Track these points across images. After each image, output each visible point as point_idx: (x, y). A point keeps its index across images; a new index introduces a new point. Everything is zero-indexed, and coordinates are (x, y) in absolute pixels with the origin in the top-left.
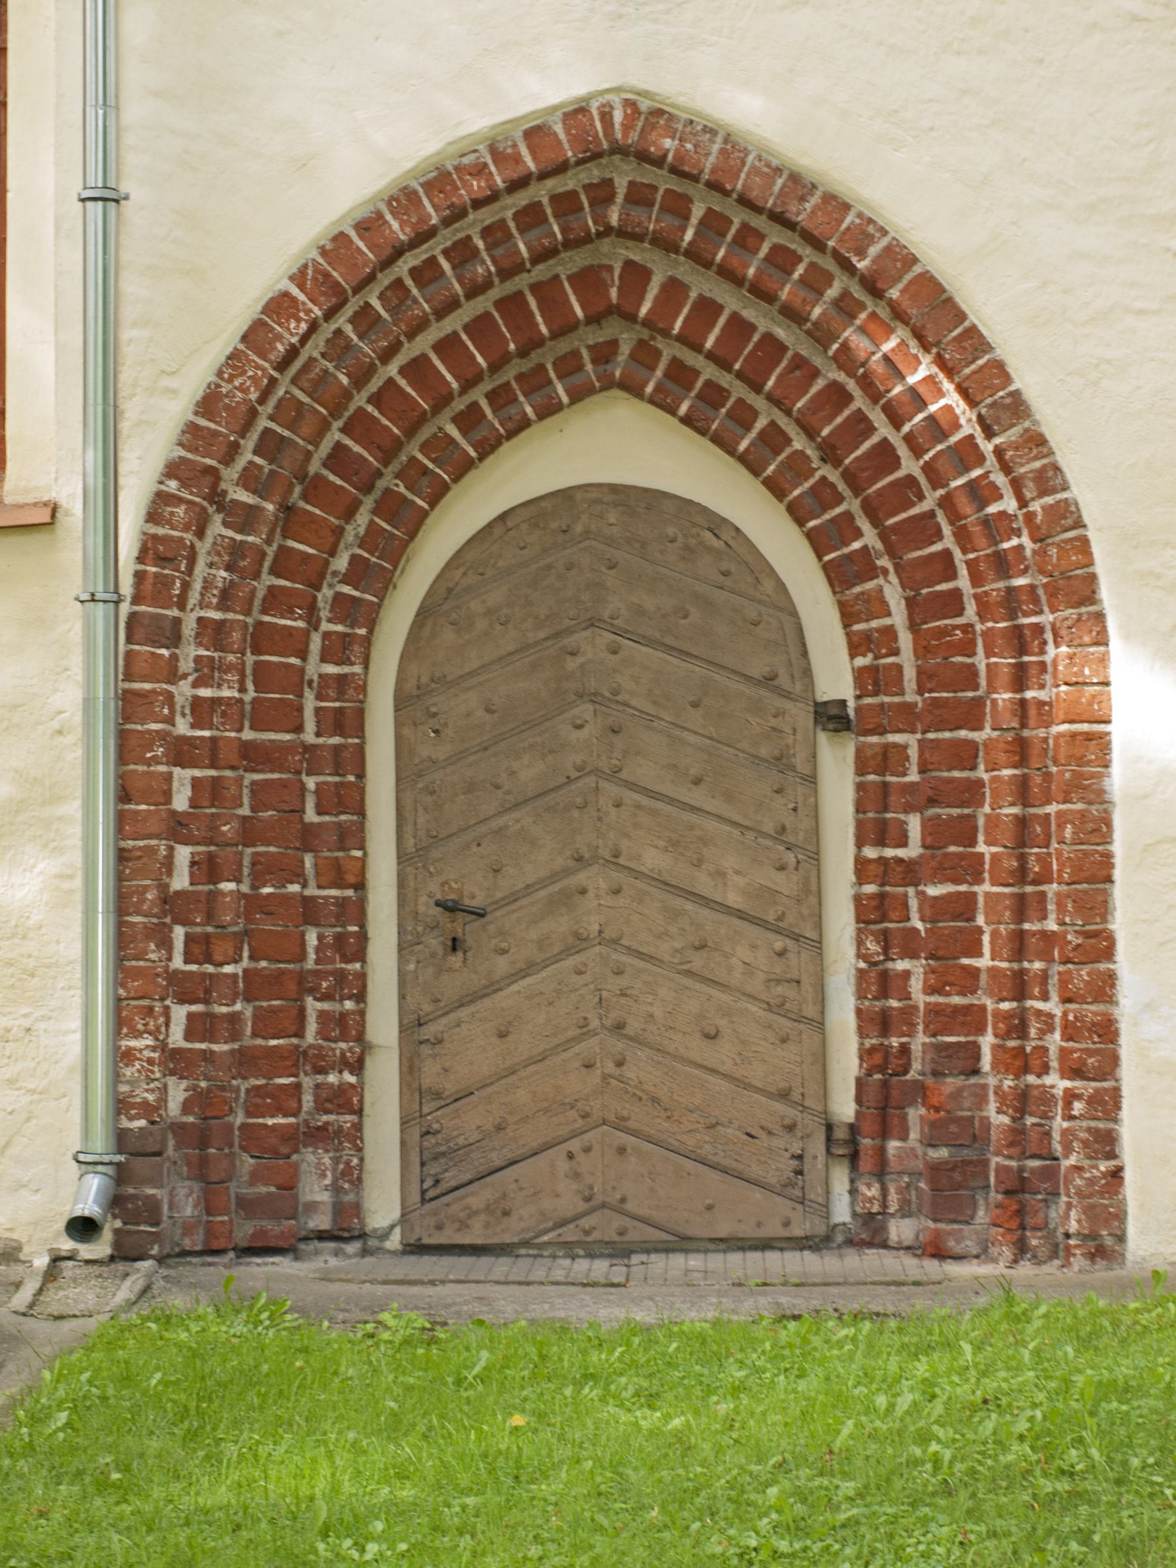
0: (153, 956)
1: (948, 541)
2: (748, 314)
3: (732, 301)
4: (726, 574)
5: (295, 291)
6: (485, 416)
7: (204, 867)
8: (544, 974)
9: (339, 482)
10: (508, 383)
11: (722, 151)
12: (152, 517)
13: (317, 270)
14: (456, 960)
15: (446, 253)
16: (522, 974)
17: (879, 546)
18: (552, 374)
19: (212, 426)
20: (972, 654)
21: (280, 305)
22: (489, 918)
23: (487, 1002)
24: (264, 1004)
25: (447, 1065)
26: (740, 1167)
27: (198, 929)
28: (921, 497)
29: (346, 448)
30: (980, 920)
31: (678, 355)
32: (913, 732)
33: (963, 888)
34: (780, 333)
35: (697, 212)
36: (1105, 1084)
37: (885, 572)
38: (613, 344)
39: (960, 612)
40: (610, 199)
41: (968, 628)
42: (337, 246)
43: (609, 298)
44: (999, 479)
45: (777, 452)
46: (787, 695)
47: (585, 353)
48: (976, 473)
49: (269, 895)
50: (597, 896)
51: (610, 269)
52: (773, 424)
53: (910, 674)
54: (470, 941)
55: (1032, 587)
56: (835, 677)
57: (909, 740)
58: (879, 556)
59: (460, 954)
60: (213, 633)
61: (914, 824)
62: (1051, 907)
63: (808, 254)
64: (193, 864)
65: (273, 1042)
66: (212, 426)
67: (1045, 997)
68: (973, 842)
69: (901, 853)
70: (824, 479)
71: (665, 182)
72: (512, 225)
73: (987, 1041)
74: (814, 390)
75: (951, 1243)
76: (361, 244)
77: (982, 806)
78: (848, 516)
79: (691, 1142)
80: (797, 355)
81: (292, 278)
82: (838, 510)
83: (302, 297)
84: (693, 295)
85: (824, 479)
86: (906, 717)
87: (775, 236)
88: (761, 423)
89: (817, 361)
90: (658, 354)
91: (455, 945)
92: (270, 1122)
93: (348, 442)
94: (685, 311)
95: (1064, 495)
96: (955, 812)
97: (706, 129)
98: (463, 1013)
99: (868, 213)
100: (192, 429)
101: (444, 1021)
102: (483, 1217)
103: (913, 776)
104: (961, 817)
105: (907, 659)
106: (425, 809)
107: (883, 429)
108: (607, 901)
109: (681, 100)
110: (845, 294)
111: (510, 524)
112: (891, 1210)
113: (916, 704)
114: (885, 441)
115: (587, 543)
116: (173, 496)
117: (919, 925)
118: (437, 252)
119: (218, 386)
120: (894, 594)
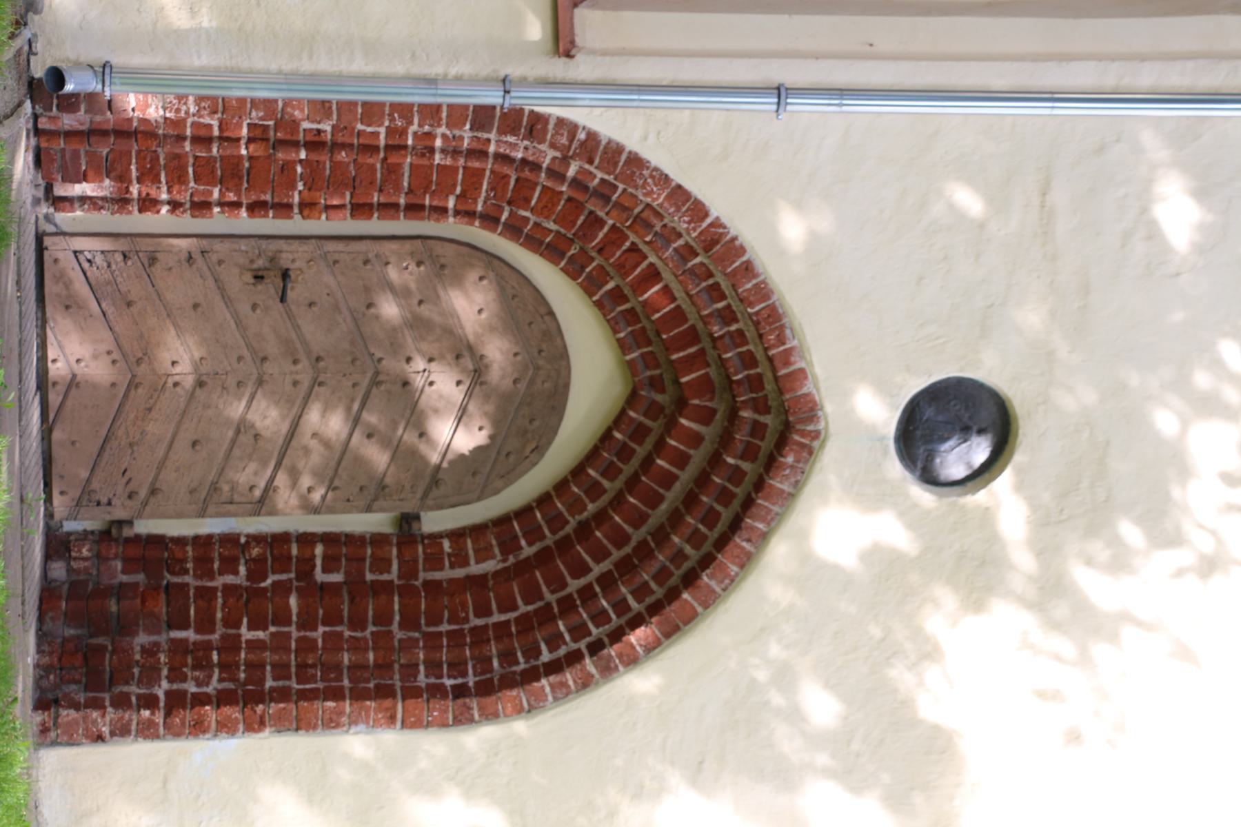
0: (254, 114)
1: (523, 608)
2: (677, 487)
3: (685, 477)
4: (508, 455)
5: (708, 221)
6: (620, 305)
7: (316, 139)
8: (238, 336)
9: (579, 222)
10: (640, 322)
11: (782, 491)
12: (561, 122)
13: (721, 234)
14: (248, 277)
15: (729, 307)
16: (239, 323)
17: (522, 557)
18: (645, 350)
19: (621, 164)
20: (450, 622)
21: (698, 210)
22: (280, 305)
23: (218, 298)
24: (218, 165)
25: (174, 270)
26: (102, 465)
27: (272, 133)
28: (553, 592)
29: (602, 228)
30: (272, 629)
31: (653, 433)
32: (400, 577)
33: (294, 618)
34: (664, 507)
35: (746, 466)
36: (161, 729)
37: (504, 561)
38: (662, 390)
39: (477, 615)
40: (756, 410)
41: (466, 620)
42: (735, 249)
43: (694, 398)
44: (562, 651)
45: (586, 493)
46: (425, 495)
47: (658, 372)
48: (567, 637)
49: (296, 171)
50: (291, 373)
51: (711, 399)
52: (605, 491)
53: (437, 575)
54: (260, 287)
55: (491, 670)
56: (434, 521)
57: (393, 575)
58: (515, 557)
59: (252, 281)
60: (478, 153)
61: (337, 578)
62: (281, 683)
63: (714, 535)
64: (319, 131)
65: (190, 170)
66: (621, 164)
67: (221, 680)
68: (324, 624)
69: (318, 568)
70: (567, 522)
71: (766, 445)
72: (744, 349)
73: (190, 635)
74: (626, 526)
75: (50, 614)
76: (737, 264)
77: (349, 630)
78: (543, 537)
79: (120, 433)
80: (648, 516)
81: (717, 218)
82: (546, 531)
83: (704, 225)
84: (692, 452)
85: (567, 522)
86: (409, 571)
87: (726, 515)
88: (606, 483)
89: (644, 529)
90: (654, 419)
91: (259, 278)
92: (133, 167)
93: (606, 229)
94: (682, 447)
95: (550, 698)
96: (346, 613)
97: (797, 482)
98: (210, 282)
99: (737, 579)
100: (619, 149)
101: (205, 268)
102: (64, 292)
103: (369, 577)
104: (342, 617)
105: (447, 574)
106: (354, 259)
107: (597, 569)
108: (289, 379)
109: (818, 466)
110: (686, 557)
111: (546, 318)
112: (72, 563)
113: (417, 579)
114: (590, 570)
115: (531, 367)
116: (574, 137)
117: (269, 581)
118: (729, 300)
119: (648, 168)
120: (490, 566)
